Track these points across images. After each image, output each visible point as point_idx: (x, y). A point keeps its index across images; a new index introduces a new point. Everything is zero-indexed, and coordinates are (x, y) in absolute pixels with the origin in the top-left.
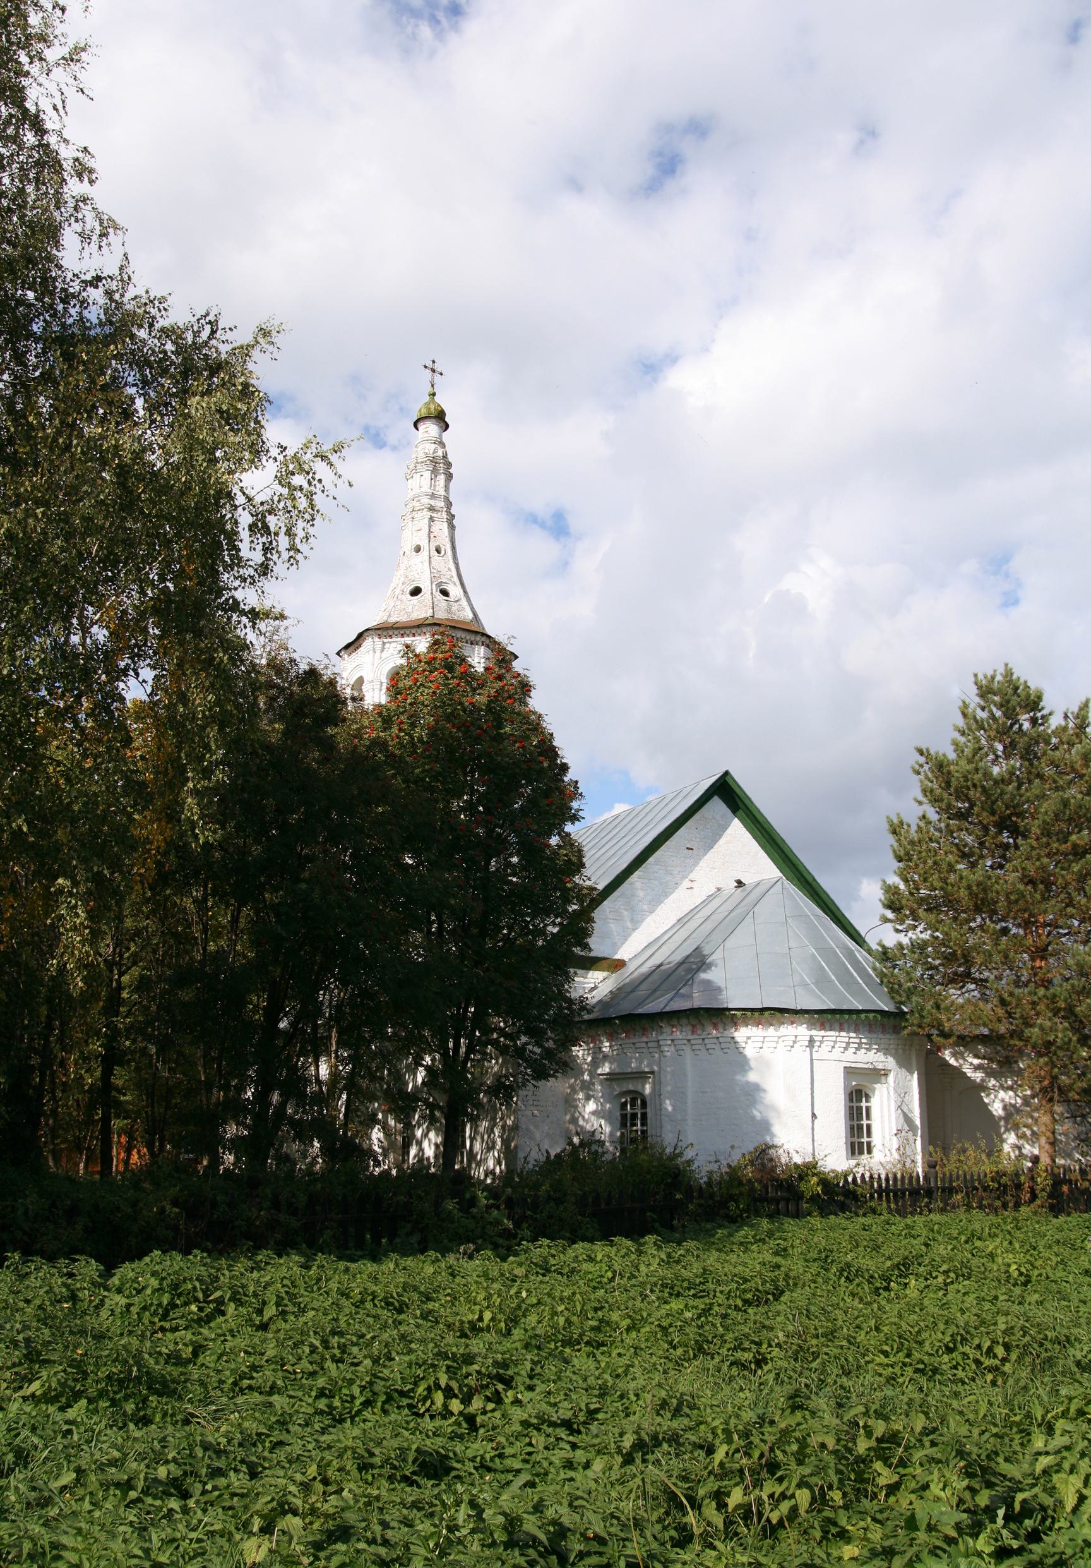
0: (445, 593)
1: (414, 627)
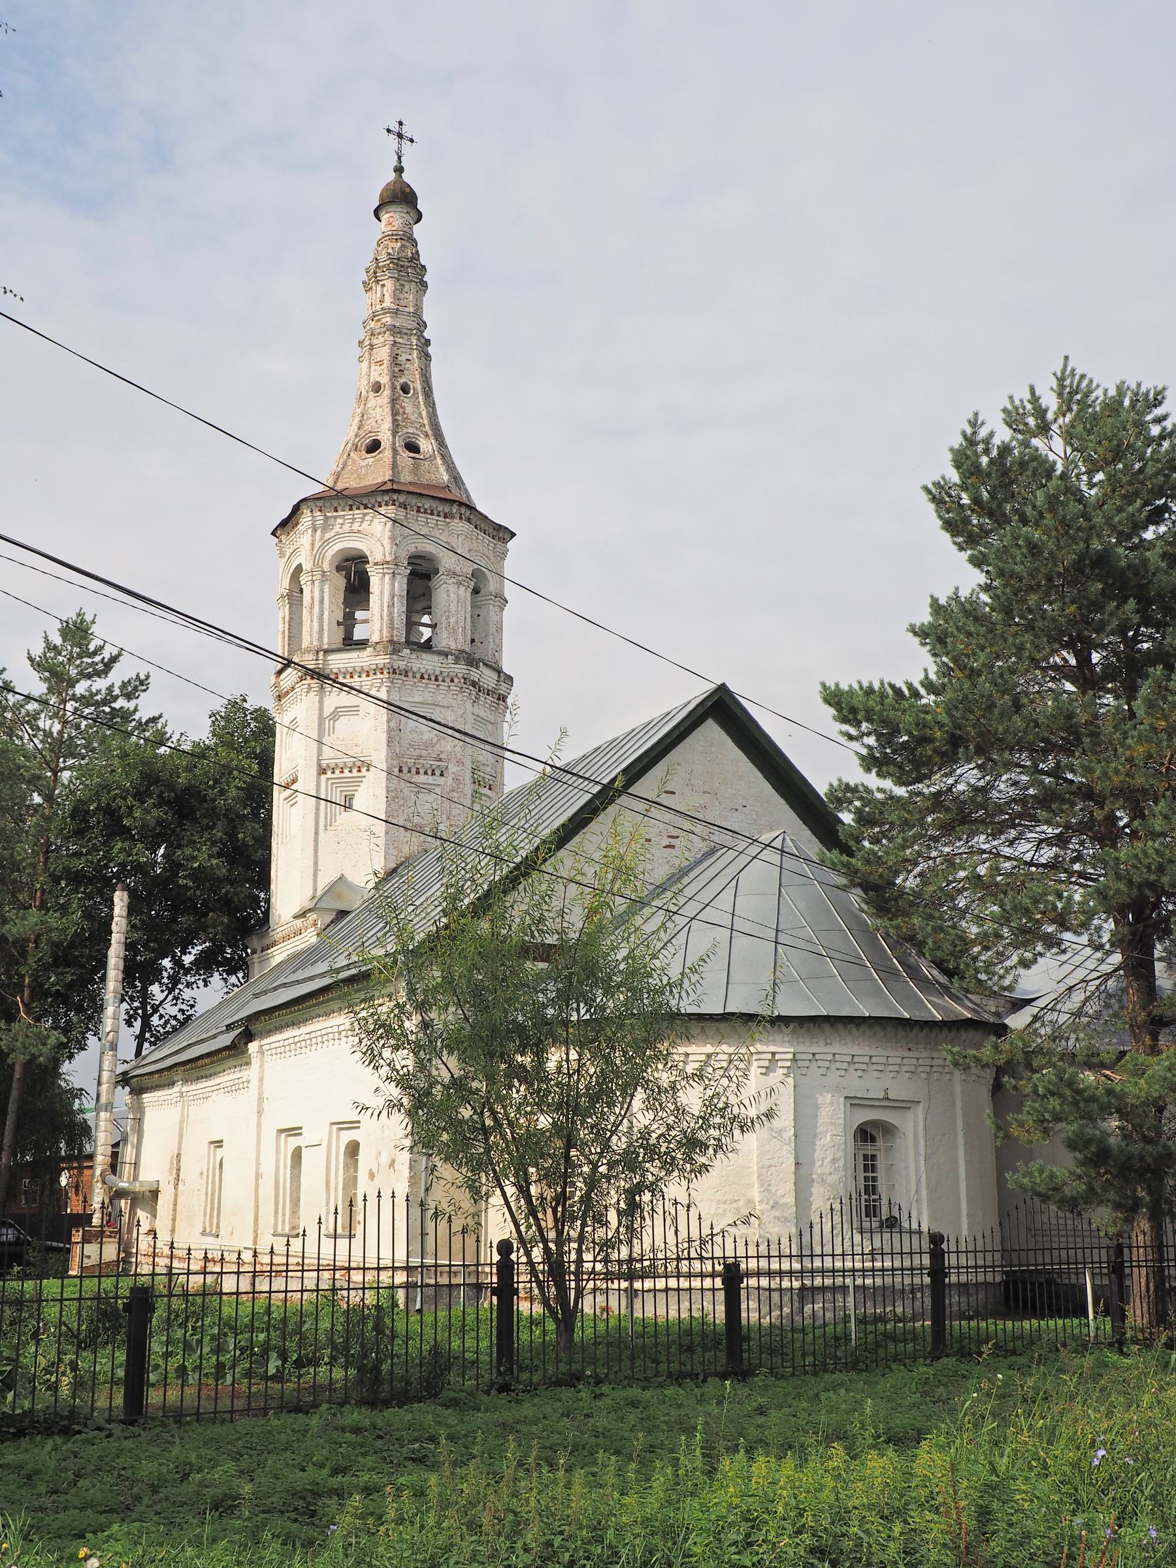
0: (412, 447)
1: (367, 495)
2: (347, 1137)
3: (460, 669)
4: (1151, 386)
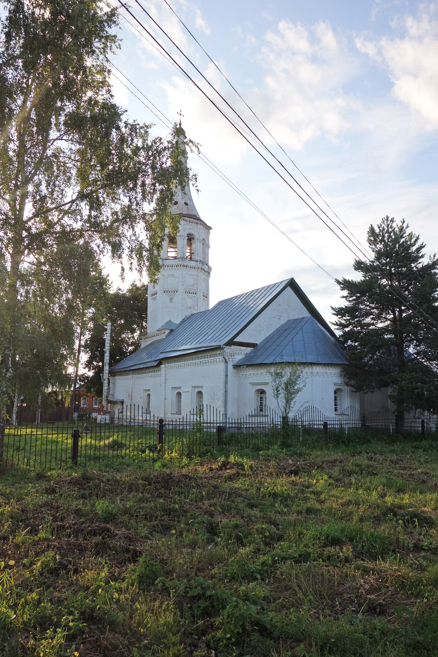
2: (147, 393)
3: (200, 265)
4: (379, 222)
